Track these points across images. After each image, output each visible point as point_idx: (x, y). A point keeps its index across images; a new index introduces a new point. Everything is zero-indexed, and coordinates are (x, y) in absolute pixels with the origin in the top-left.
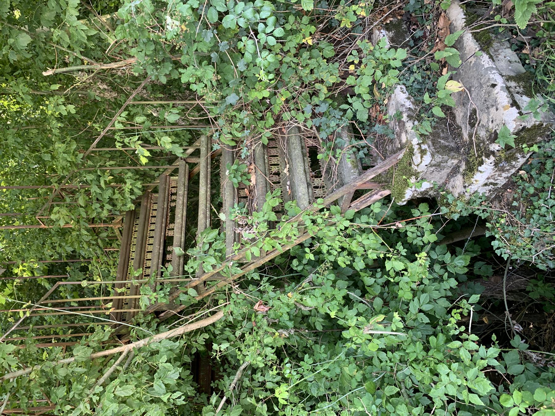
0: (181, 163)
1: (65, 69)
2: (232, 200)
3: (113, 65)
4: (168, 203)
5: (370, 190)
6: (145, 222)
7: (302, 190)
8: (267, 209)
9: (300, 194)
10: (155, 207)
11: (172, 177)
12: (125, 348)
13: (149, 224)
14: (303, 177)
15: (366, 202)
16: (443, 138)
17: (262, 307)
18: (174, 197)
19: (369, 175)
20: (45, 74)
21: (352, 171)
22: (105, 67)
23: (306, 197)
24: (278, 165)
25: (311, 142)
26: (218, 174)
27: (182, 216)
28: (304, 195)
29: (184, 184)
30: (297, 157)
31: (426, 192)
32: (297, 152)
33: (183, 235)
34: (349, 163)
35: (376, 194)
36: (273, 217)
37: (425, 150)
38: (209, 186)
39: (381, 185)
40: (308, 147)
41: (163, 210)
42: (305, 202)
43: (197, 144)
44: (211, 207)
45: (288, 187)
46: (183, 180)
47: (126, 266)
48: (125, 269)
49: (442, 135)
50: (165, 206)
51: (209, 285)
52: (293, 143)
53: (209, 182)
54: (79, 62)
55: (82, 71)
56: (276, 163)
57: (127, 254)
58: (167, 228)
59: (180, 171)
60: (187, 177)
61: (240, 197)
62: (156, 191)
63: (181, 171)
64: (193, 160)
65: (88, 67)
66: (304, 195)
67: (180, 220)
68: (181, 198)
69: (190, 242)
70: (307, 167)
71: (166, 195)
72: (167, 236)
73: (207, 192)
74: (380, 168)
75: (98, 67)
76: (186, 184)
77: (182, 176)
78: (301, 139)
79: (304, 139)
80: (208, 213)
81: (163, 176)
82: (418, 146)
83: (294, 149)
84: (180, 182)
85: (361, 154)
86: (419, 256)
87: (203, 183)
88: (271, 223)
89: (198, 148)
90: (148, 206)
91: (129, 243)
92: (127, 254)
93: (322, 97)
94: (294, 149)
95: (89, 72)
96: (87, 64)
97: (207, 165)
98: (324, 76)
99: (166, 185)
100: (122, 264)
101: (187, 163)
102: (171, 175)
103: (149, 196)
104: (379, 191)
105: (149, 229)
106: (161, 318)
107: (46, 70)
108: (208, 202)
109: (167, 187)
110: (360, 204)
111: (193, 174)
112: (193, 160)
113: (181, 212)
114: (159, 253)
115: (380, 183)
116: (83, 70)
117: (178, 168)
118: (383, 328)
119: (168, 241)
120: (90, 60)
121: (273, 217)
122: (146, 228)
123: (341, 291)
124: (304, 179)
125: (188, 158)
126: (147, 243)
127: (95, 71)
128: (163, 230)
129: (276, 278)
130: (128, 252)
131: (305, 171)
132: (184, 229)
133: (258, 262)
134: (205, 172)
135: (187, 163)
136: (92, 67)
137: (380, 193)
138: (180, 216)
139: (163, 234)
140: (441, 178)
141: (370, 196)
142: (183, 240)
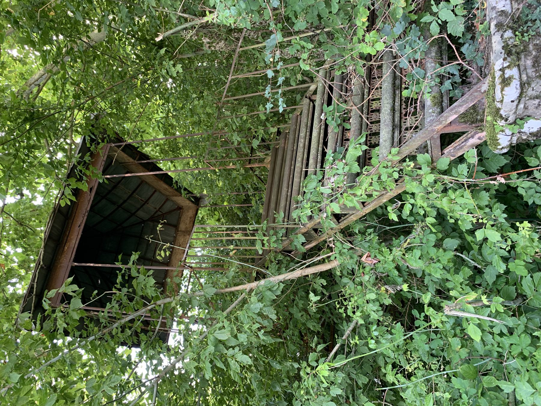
5: (463, 133)
8: (351, 159)
15: (461, 148)
19: (447, 117)
20: (158, 40)
21: (431, 111)
34: (429, 100)
35: (472, 137)
36: (356, 168)
37: (510, 78)
42: (384, 151)
54: (182, 20)
55: (186, 29)
61: (155, 191)
68: (302, 141)
73: (320, 134)
82: (501, 73)
86: (522, 225)
95: (193, 27)
96: (190, 21)
99: (296, 126)
104: (476, 133)
110: (452, 151)
113: (301, 156)
114: (287, 195)
115: (473, 122)
116: (186, 27)
118: (473, 310)
123: (447, 253)
127: (197, 26)
133: (358, 213)
137: (477, 136)
141: (466, 141)
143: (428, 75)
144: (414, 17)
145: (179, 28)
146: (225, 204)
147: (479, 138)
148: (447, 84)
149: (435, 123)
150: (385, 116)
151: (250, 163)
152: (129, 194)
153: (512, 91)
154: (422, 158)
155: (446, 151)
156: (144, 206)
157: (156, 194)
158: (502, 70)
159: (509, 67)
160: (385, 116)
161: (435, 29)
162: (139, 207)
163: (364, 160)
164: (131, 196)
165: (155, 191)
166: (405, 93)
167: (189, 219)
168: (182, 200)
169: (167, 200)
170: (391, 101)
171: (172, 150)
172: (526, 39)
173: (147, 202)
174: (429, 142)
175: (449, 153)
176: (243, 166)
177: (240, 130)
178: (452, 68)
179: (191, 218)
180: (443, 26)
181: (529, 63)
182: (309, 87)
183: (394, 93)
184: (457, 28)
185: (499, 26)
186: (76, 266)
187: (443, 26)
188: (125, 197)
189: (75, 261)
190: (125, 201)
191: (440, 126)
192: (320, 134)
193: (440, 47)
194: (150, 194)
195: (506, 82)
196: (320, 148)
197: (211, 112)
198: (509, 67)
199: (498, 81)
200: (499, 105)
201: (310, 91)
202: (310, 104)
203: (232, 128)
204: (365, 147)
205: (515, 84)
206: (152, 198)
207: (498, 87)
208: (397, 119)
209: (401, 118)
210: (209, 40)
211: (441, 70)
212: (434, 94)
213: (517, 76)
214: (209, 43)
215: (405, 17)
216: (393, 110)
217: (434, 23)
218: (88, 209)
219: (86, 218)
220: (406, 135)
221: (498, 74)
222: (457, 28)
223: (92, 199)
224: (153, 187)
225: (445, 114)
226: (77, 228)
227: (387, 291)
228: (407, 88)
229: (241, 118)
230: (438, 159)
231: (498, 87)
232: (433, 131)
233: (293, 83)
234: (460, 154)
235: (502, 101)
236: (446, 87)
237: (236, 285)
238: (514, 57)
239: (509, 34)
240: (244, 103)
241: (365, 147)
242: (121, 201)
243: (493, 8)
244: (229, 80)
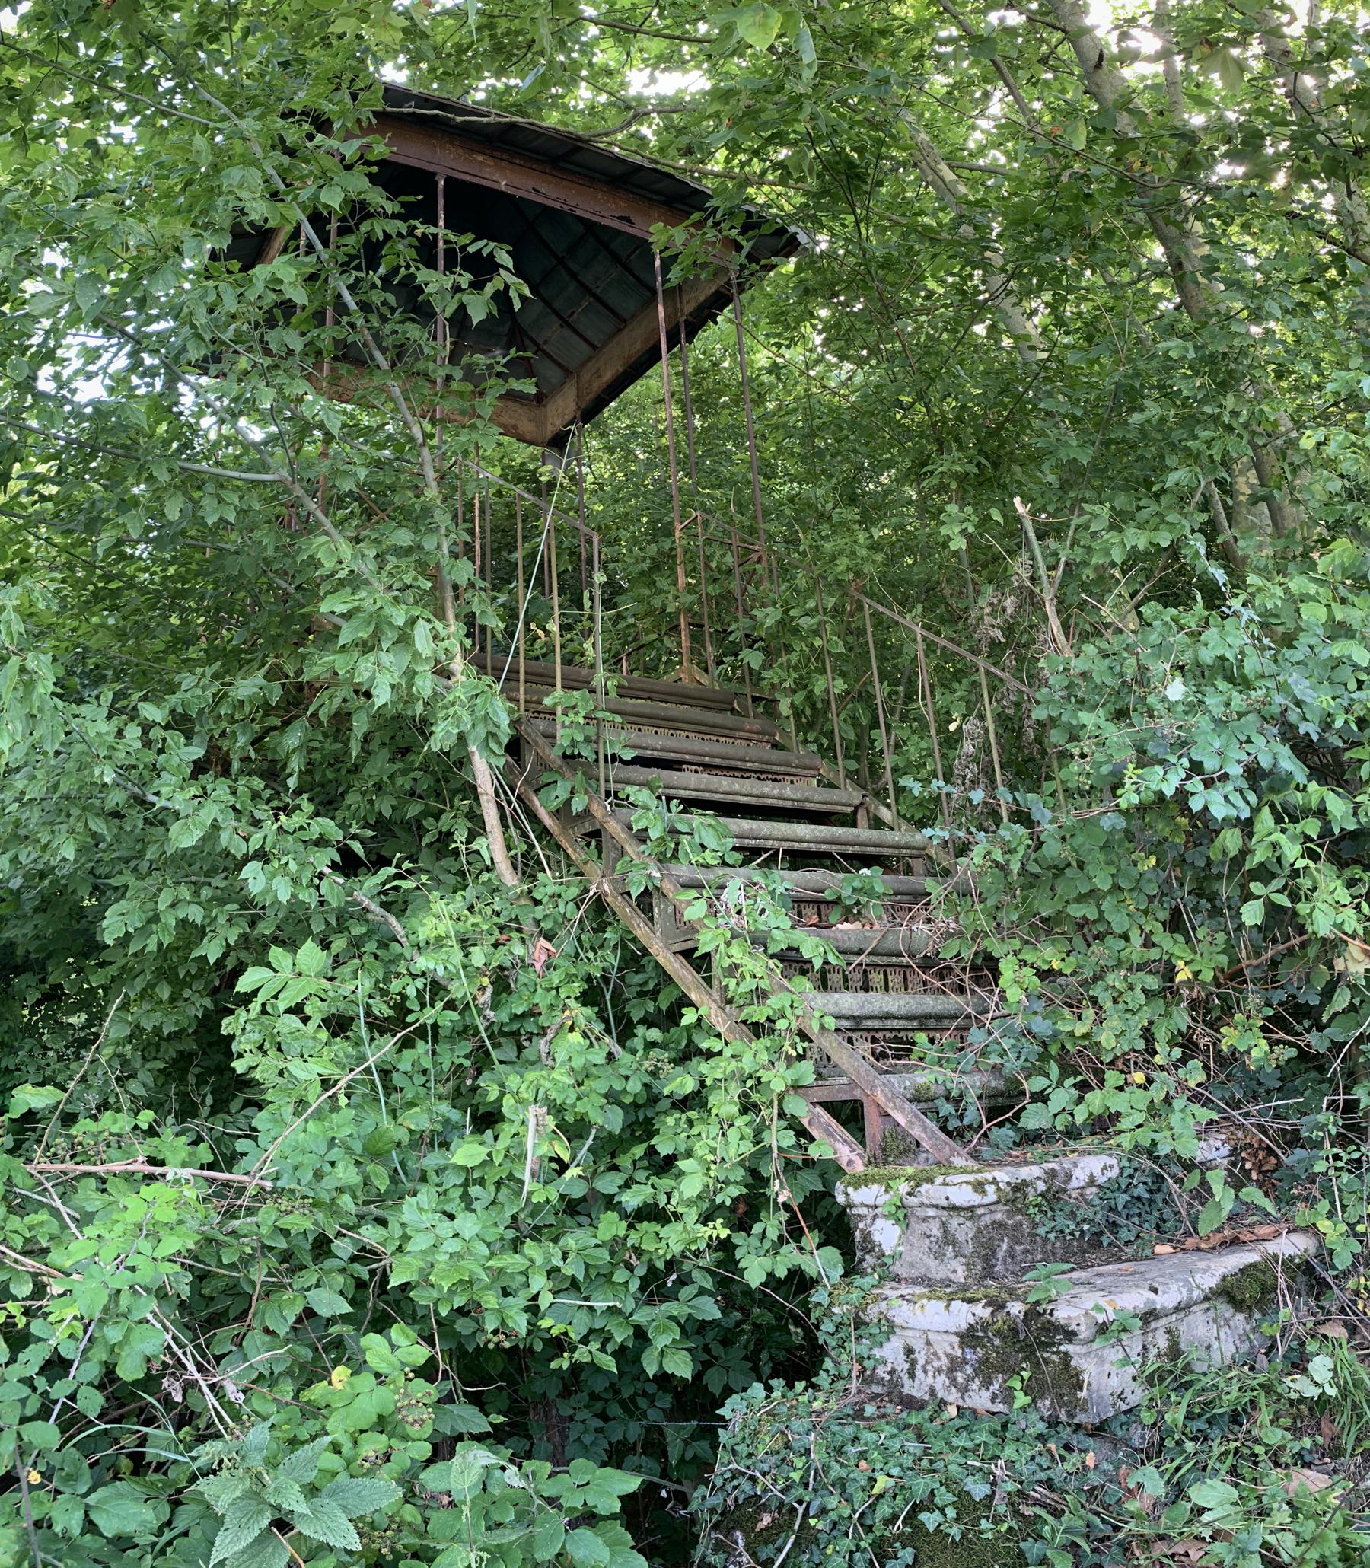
1: (1032, 535)
3: (1055, 624)
16: (1011, 1249)
17: (544, 957)
19: (902, 1110)
20: (1017, 500)
22: (1050, 609)
29: (807, 801)
31: (869, 1245)
37: (984, 1192)
44: (766, 850)
49: (1019, 1248)
51: (588, 845)
53: (823, 847)
54: (1052, 561)
61: (594, 347)
65: (1045, 578)
68: (776, 792)
73: (800, 841)
74: (925, 1129)
75: (1048, 595)
76: (809, 806)
80: (752, 843)
81: (818, 761)
97: (860, 845)
98: (1113, 1023)
101: (856, 808)
107: (1024, 502)
109: (793, 771)
115: (884, 1150)
120: (1058, 581)
128: (697, 759)
134: (843, 839)
135: (856, 808)
136: (1045, 584)
138: (736, 787)
140: (912, 1265)
143: (964, 1078)
144: (1054, 1050)
145: (1038, 553)
147: (850, 1162)
148: (947, 1109)
149: (889, 1094)
150: (878, 1002)
152: (593, 287)
153: (963, 1196)
154: (806, 1071)
155: (819, 1110)
156: (554, 318)
157: (585, 348)
158: (995, 1182)
159: (999, 1189)
160: (878, 1002)
161: (1037, 1084)
162: (556, 305)
163: (792, 961)
164: (589, 291)
165: (594, 347)
166: (921, 1038)
167: (512, 422)
168: (563, 407)
169: (567, 372)
170: (903, 1012)
171: (699, 395)
172: (1031, 1211)
173: (566, 323)
174: (845, 1080)
175: (819, 1116)
177: (786, 625)
178: (974, 1113)
179: (515, 427)
180: (1041, 1097)
181: (998, 1216)
183: (914, 1018)
184: (1034, 1118)
185: (1052, 1174)
186: (436, 183)
187: (1041, 1097)
188: (587, 278)
189: (449, 180)
190: (574, 276)
191: (881, 1098)
192: (800, 841)
193: (1002, 1094)
194: (589, 334)
195: (979, 1187)
198: (999, 1189)
199: (979, 1176)
200: (939, 1180)
204: (818, 963)
205: (976, 1199)
206: (575, 338)
207: (971, 1178)
208: (870, 1024)
209: (868, 1030)
211: (971, 1097)
212: (933, 1087)
213: (987, 1200)
215: (1056, 1034)
216: (888, 1016)
218: (579, 213)
219: (557, 205)
221: (989, 1177)
222: (1034, 1118)
223: (604, 222)
224: (605, 344)
225: (908, 1106)
226: (530, 184)
228: (932, 1041)
230: (805, 1096)
231: (971, 1178)
232: (873, 1088)
234: (815, 1133)
235: (945, 1184)
238: (1010, 1196)
239: (1041, 1187)
241: (818, 963)
242: (575, 267)
243: (1075, 1165)
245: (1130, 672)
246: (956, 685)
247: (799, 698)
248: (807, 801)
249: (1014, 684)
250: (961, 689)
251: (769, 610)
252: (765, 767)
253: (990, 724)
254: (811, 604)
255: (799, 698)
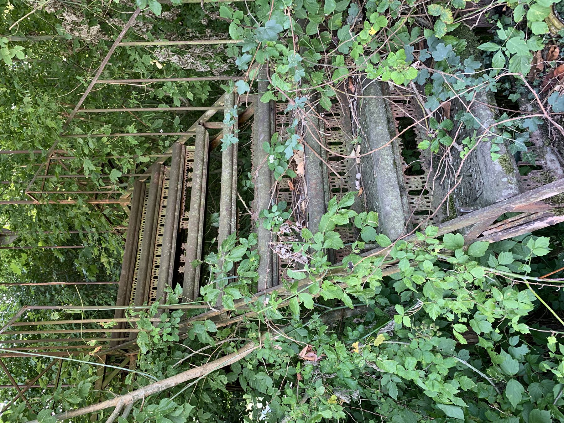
0: (198, 129)
2: (268, 196)
4: (183, 182)
6: (155, 206)
7: (392, 201)
8: (328, 227)
9: (388, 208)
10: (168, 184)
11: (188, 147)
12: (118, 402)
13: (161, 208)
14: (392, 175)
17: (312, 354)
18: (190, 175)
19: (545, 193)
21: (505, 180)
23: (400, 214)
24: (341, 143)
25: (402, 111)
26: (249, 148)
27: (200, 205)
28: (395, 210)
29: (203, 160)
30: (380, 138)
32: (379, 128)
33: (200, 233)
38: (235, 167)
39: (557, 206)
40: (397, 119)
41: (177, 193)
43: (219, 103)
44: (238, 197)
45: (357, 183)
46: (201, 154)
47: (133, 259)
48: (132, 264)
50: (179, 187)
52: (373, 113)
56: (337, 140)
57: (135, 244)
58: (182, 217)
59: (197, 141)
60: (206, 149)
62: (167, 163)
63: (199, 141)
64: (214, 125)
66: (395, 210)
67: (197, 212)
68: (198, 180)
69: (209, 244)
70: (398, 156)
71: (181, 171)
72: (182, 229)
76: (206, 160)
77: (200, 148)
78: (386, 105)
79: (391, 105)
80: (234, 208)
81: (177, 145)
83: (375, 122)
84: (198, 154)
85: (519, 143)
87: (227, 162)
88: (332, 252)
89: (220, 108)
90: (160, 184)
91: (137, 228)
92: (135, 244)
93: (441, 30)
94: (375, 122)
99: (180, 158)
100: (128, 257)
102: (186, 144)
103: (160, 170)
105: (161, 214)
106: (167, 356)
108: (234, 192)
109: (182, 160)
111: (215, 143)
112: (214, 125)
113: (198, 201)
114: (170, 253)
117: (195, 136)
119: (182, 236)
121: (336, 242)
122: (156, 213)
124: (394, 181)
125: (208, 121)
126: (158, 233)
128: (176, 220)
129: (332, 309)
130: (135, 241)
131: (395, 163)
132: (201, 225)
139: (175, 226)
142: (200, 240)
146: (40, 244)
151: (96, 198)
176: (87, 202)
182: (203, 112)
196: (233, 195)
197: (54, 126)
201: (206, 117)
202: (205, 133)
203: (83, 151)
210: (75, 19)
214: (74, 23)
217: (500, 54)
220: (413, 201)
227: (338, 399)
229: (99, 139)
233: (177, 102)
236: (517, 147)
237: (98, 400)
240: (103, 119)
244: (92, 84)
245: (240, 62)
246: (132, 58)
247: (138, 152)
248: (203, 160)
249: (132, 22)
250: (134, 56)
251: (85, 166)
252: (180, 178)
253: (158, 43)
254: (81, 141)
255: (138, 152)
